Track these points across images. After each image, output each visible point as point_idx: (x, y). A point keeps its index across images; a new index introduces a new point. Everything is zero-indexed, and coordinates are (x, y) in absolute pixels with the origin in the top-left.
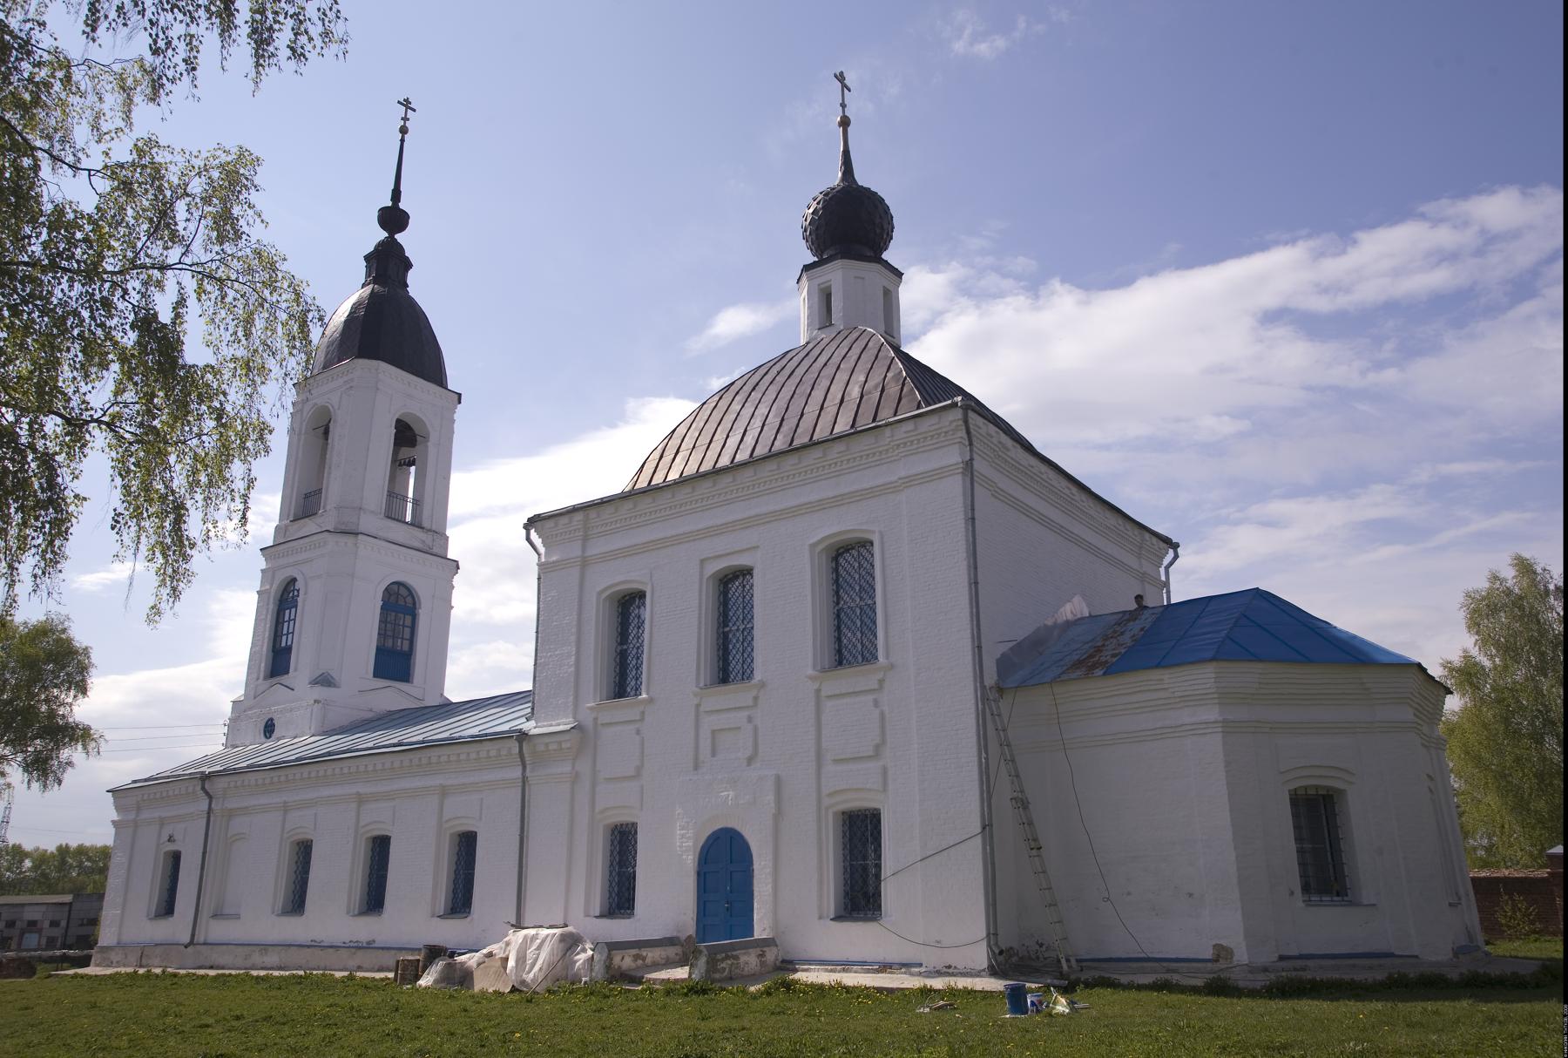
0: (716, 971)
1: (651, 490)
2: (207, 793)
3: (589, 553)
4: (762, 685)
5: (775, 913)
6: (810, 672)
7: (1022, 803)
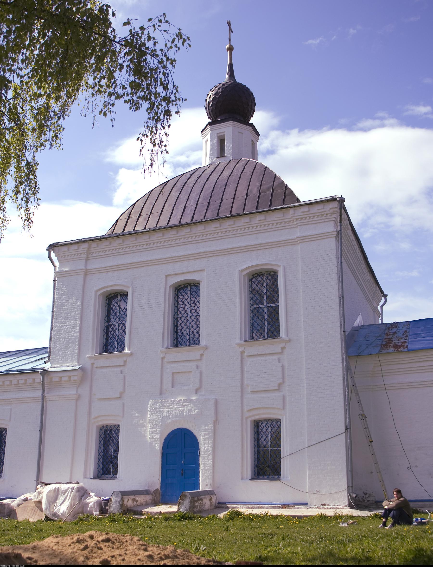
0: (195, 507)
1: (123, 235)
3: (89, 267)
4: (206, 348)
5: (213, 476)
6: (238, 341)
7: (363, 416)
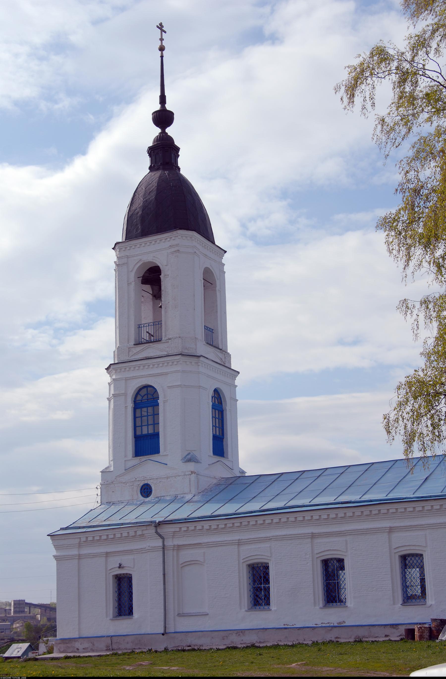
2: (160, 536)
